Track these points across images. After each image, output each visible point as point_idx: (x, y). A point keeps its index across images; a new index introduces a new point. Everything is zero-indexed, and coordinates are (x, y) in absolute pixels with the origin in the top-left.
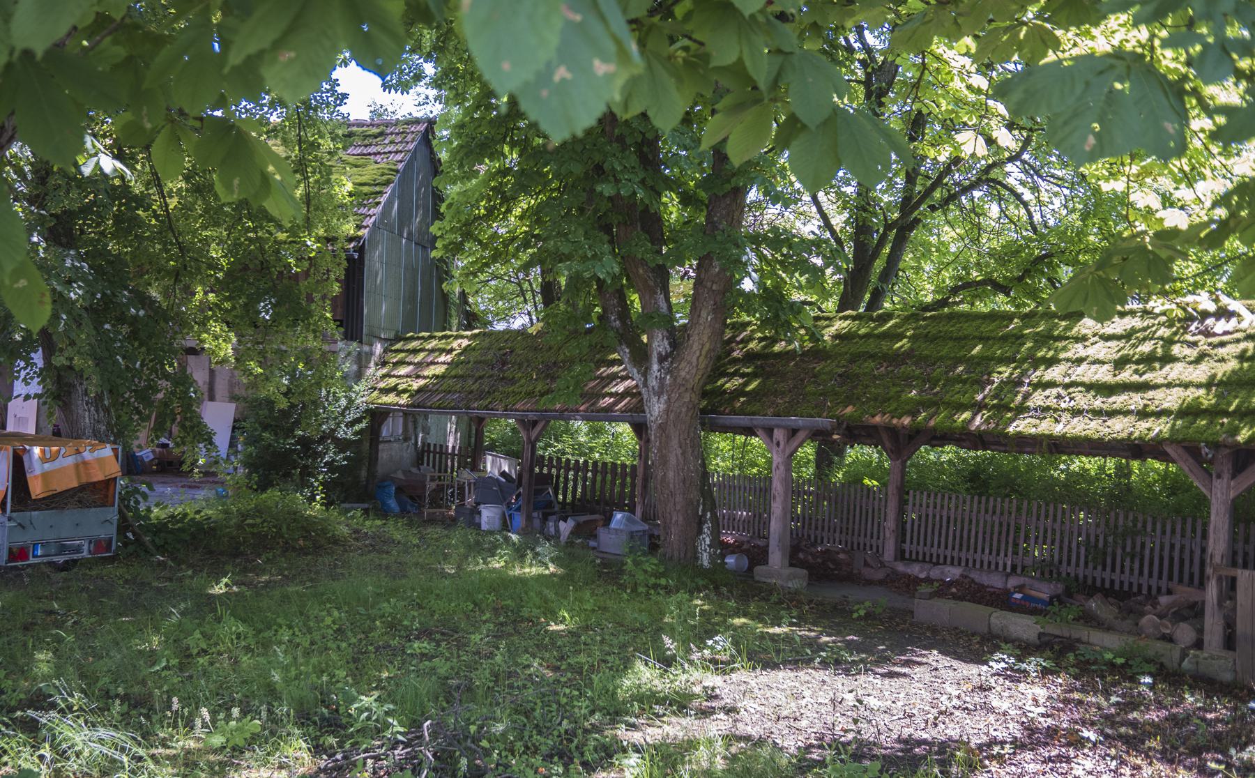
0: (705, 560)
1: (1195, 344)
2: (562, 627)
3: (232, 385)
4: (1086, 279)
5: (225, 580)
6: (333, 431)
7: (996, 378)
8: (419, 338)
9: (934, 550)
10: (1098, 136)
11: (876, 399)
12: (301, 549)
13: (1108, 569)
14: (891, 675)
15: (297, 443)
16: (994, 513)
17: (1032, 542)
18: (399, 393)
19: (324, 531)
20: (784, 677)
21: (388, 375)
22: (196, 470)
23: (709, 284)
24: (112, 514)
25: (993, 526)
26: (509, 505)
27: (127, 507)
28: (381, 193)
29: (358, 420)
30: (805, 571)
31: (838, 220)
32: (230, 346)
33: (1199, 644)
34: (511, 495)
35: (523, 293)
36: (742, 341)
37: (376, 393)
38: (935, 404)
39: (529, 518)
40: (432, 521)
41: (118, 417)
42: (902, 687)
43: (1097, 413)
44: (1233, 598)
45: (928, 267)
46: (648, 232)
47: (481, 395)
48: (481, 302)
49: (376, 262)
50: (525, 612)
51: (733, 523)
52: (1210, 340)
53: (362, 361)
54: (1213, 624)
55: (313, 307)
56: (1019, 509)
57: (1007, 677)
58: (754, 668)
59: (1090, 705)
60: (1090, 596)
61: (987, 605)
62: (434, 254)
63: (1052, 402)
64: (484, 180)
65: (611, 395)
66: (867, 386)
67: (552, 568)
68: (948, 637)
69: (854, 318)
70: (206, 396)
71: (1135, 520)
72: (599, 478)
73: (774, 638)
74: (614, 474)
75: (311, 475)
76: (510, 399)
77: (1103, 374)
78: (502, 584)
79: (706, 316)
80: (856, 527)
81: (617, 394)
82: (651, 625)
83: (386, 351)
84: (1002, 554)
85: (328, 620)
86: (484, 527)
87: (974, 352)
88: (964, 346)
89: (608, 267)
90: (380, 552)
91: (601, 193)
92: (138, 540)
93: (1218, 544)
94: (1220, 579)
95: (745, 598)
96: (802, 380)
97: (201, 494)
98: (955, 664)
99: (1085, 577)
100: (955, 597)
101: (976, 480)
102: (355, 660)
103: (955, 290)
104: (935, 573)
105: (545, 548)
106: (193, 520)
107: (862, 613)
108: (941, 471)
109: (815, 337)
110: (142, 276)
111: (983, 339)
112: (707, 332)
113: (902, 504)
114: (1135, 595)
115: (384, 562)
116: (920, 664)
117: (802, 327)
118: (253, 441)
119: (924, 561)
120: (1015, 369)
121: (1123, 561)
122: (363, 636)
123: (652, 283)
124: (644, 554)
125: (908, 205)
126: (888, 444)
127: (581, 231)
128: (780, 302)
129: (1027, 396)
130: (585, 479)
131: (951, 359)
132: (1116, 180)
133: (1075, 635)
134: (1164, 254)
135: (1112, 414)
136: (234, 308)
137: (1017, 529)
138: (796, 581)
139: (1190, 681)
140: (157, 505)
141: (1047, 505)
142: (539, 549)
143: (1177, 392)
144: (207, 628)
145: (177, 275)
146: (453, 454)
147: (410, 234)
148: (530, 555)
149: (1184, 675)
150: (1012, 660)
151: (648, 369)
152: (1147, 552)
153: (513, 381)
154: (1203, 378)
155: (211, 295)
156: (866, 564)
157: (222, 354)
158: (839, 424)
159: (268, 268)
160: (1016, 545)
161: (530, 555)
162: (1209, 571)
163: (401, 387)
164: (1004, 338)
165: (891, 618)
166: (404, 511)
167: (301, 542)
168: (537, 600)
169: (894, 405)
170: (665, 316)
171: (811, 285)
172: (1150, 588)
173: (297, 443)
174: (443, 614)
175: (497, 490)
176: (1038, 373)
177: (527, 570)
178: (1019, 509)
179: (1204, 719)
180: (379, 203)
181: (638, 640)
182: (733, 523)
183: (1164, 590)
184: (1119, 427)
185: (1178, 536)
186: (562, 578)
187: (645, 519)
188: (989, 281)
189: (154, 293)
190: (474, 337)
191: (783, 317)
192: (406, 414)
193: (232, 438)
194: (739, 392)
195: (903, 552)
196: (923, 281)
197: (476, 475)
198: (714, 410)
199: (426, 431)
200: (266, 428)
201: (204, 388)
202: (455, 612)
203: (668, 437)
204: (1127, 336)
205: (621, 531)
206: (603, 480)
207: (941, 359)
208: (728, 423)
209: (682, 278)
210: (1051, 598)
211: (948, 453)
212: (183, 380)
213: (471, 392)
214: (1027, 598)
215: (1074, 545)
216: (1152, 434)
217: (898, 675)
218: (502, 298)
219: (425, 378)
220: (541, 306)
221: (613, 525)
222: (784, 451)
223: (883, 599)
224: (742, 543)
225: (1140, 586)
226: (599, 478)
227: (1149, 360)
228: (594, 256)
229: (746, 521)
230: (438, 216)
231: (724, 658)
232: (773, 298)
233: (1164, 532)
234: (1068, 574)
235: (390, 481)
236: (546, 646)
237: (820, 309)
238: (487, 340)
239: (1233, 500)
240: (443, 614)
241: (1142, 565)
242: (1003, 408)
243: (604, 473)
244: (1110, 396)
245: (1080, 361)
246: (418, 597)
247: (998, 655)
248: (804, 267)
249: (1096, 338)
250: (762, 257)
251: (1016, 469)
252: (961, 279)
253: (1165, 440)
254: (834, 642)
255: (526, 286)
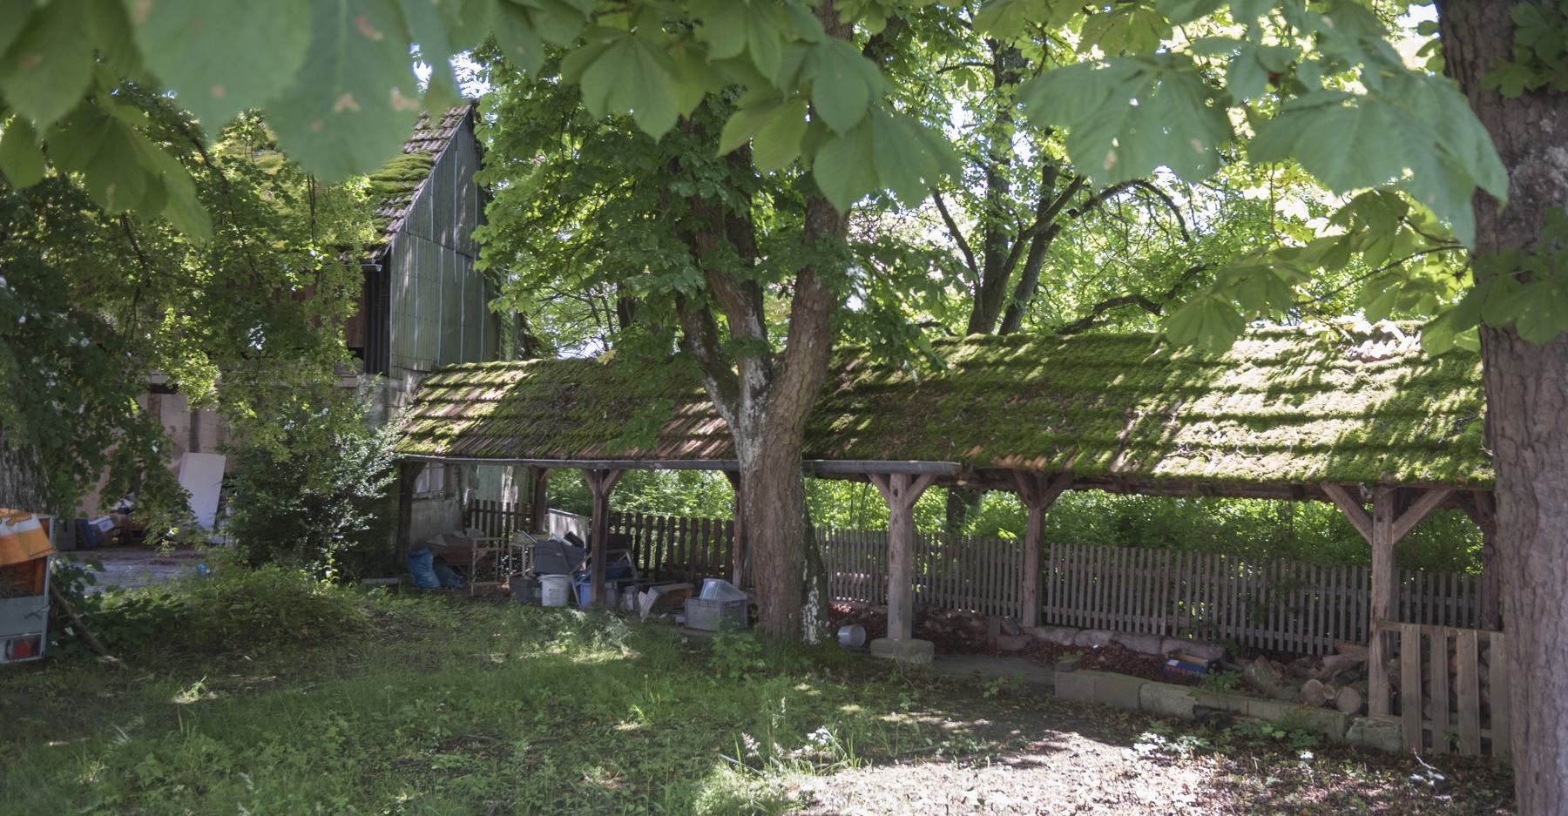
0: (812, 635)
1: (1352, 370)
2: (633, 726)
3: (222, 431)
4: (1201, 303)
5: (198, 685)
6: (352, 487)
7: (1140, 410)
8: (462, 370)
9: (1080, 613)
10: (1118, 151)
11: (1006, 438)
12: (306, 639)
13: (1271, 627)
14: (1024, 765)
15: (304, 504)
16: (1145, 566)
17: (1188, 598)
18: (436, 439)
19: (336, 616)
20: (898, 775)
21: (422, 417)
22: (166, 543)
23: (809, 304)
24: (41, 604)
25: (1144, 582)
26: (577, 575)
27: (66, 594)
28: (410, 190)
29: (383, 474)
30: (930, 644)
31: (967, 227)
32: (212, 382)
33: (1364, 711)
34: (580, 561)
35: (594, 313)
36: (853, 370)
37: (407, 439)
38: (1072, 442)
39: (601, 591)
40: (477, 598)
41: (53, 477)
42: (1036, 778)
43: (1251, 450)
44: (1396, 655)
45: (1070, 281)
46: (736, 241)
47: (539, 440)
48: (543, 324)
49: (405, 277)
50: (588, 710)
51: (848, 588)
52: (1368, 365)
53: (386, 398)
54: (1378, 686)
55: (321, 332)
56: (1173, 560)
57: (1157, 761)
58: (863, 765)
59: (1244, 788)
60: (1253, 659)
61: (1139, 675)
62: (478, 266)
63: (1202, 438)
64: (537, 177)
65: (698, 437)
66: (996, 423)
67: (626, 651)
68: (1092, 716)
69: (981, 343)
70: (187, 446)
71: (1298, 572)
72: (688, 538)
73: (889, 727)
74: (707, 532)
75: (320, 544)
76: (575, 444)
77: (1255, 405)
78: (564, 674)
79: (807, 342)
80: (991, 588)
81: (704, 436)
82: (743, 717)
83: (420, 386)
84: (1155, 615)
85: (333, 731)
86: (546, 603)
87: (1117, 382)
88: (1107, 375)
89: (690, 280)
90: (409, 639)
91: (677, 194)
92: (80, 636)
93: (1381, 595)
94: (1383, 635)
95: (857, 678)
96: (922, 417)
97: (175, 573)
98: (1099, 747)
99: (1247, 638)
100: (1105, 668)
101: (1127, 528)
102: (364, 781)
103: (1099, 309)
104: (1081, 639)
105: (616, 627)
106: (158, 607)
107: (994, 691)
108: (1088, 521)
109: (937, 365)
110: (90, 294)
111: (1127, 366)
112: (809, 360)
113: (1043, 558)
114: (1300, 656)
115: (412, 652)
116: (1058, 750)
117: (922, 353)
118: (245, 502)
119: (1069, 625)
120: (1162, 400)
121: (1286, 618)
122: (378, 749)
123: (742, 303)
124: (738, 630)
125: (1046, 208)
126: (1024, 489)
127: (655, 239)
128: (894, 325)
129: (1175, 432)
130: (672, 539)
131: (1090, 389)
132: (1258, 186)
133: (1234, 706)
134: (1284, 275)
135: (1266, 450)
136: (215, 334)
137: (1171, 584)
138: (919, 654)
139: (1355, 753)
140: (108, 590)
141: (1204, 556)
142: (609, 629)
143: (1335, 424)
144: (166, 749)
145: (137, 293)
146: (508, 513)
147: (450, 239)
148: (598, 635)
149: (1348, 746)
150: (1163, 740)
151: (739, 405)
152: (1312, 607)
153: (578, 422)
154: (1361, 409)
155: (186, 318)
156: (1003, 632)
157: (202, 392)
158: (965, 468)
159: (260, 284)
160: (1171, 603)
161: (598, 635)
162: (1373, 627)
163: (438, 432)
164: (1149, 365)
165: (1029, 696)
166: (444, 587)
167: (305, 631)
168: (604, 693)
169: (1028, 444)
170: (758, 342)
171: (929, 304)
172: (1315, 647)
173: (304, 504)
174: (484, 716)
175: (563, 556)
176: (1186, 405)
177: (594, 656)
178: (1173, 560)
179: (1364, 798)
180: (409, 203)
181: (726, 738)
182: (848, 588)
183: (1330, 649)
184: (1274, 466)
185: (1344, 587)
186: (638, 663)
187: (745, 585)
188: (1137, 298)
189: (108, 316)
190: (532, 367)
191: (897, 343)
192: (447, 465)
193: (221, 499)
194: (850, 432)
195: (1044, 615)
196: (1065, 300)
197: (534, 539)
198: (818, 451)
199: (474, 484)
200: (262, 485)
201: (182, 436)
202: (499, 712)
203: (765, 488)
204: (1281, 361)
205: (714, 602)
206: (694, 542)
207: (1079, 389)
208: (836, 468)
209: (779, 296)
210: (1210, 664)
211: (1098, 498)
212: (144, 430)
213: (527, 436)
214: (1183, 664)
215: (1234, 602)
216: (1309, 473)
217: (1032, 765)
218: (570, 318)
219: (469, 419)
220: (617, 329)
221: (704, 595)
222: (903, 501)
223: (1018, 673)
224: (860, 612)
225: (1305, 646)
226: (688, 538)
227: (1302, 390)
228: (672, 268)
229: (864, 585)
230: (484, 220)
231: (829, 755)
232: (887, 321)
233: (1328, 584)
234: (1228, 635)
235: (425, 549)
236: (612, 751)
237: (948, 331)
238: (548, 372)
239: (1395, 546)
240: (484, 716)
241: (1306, 623)
242: (1151, 443)
243: (695, 532)
244: (1263, 430)
245: (1231, 390)
246: (452, 696)
247: (1147, 735)
248: (920, 282)
249: (1249, 364)
250: (872, 271)
251: (1171, 514)
252: (1105, 295)
253: (1322, 479)
254: (960, 728)
255: (599, 305)
